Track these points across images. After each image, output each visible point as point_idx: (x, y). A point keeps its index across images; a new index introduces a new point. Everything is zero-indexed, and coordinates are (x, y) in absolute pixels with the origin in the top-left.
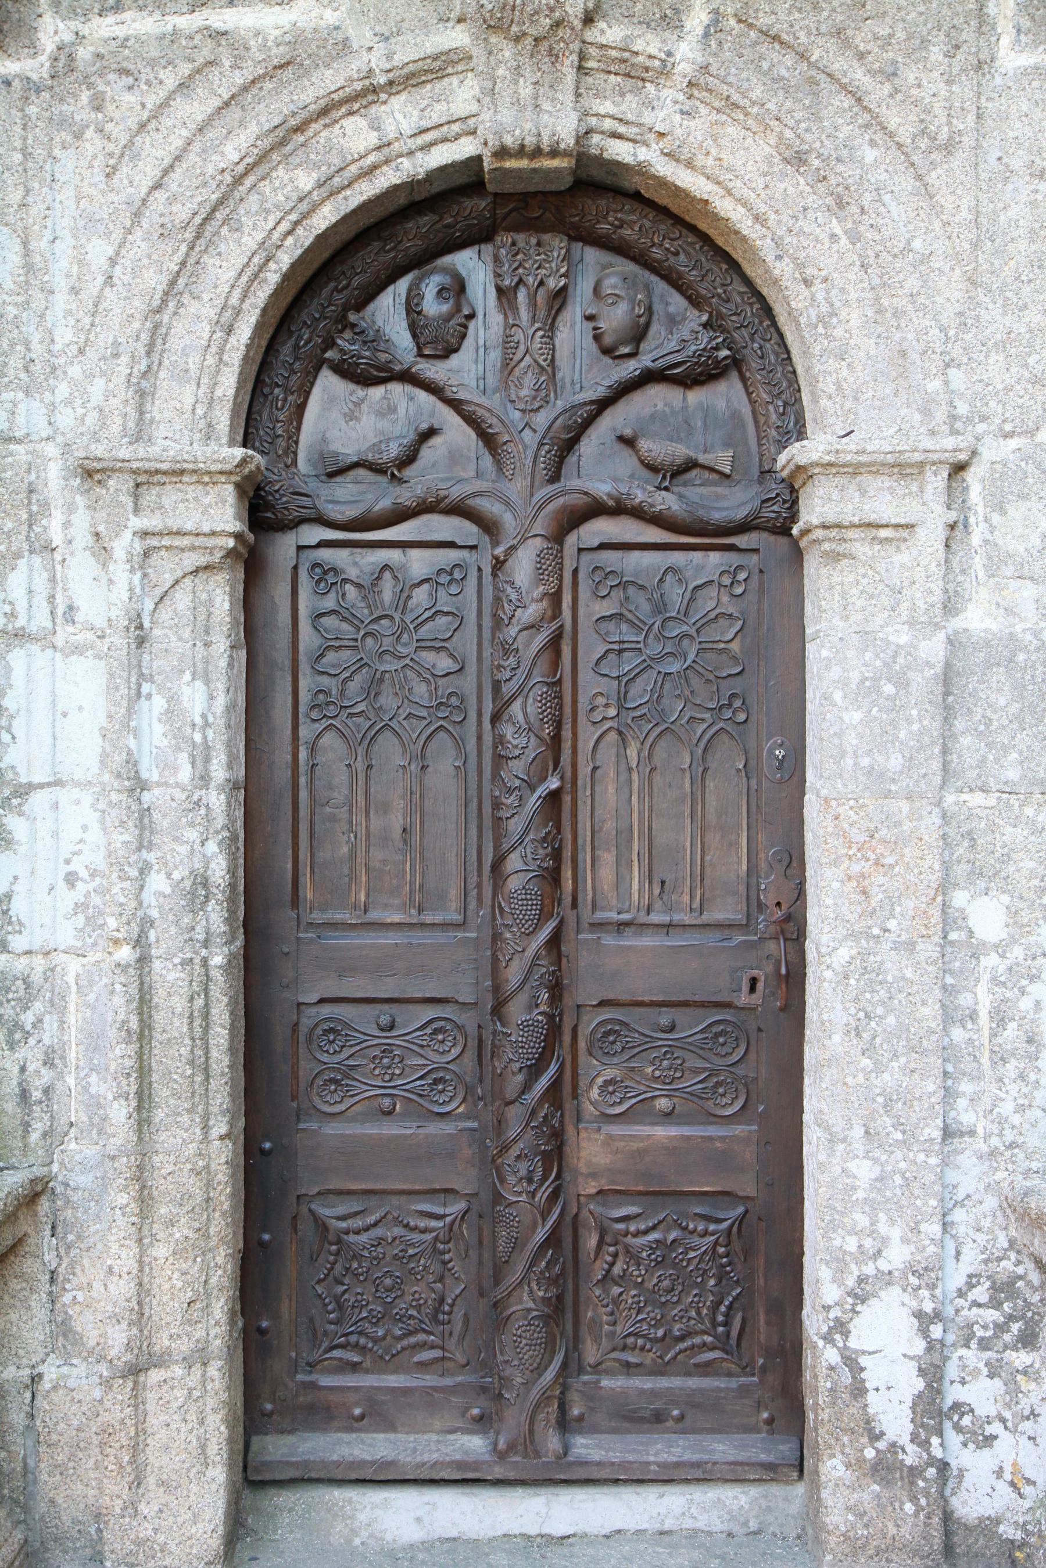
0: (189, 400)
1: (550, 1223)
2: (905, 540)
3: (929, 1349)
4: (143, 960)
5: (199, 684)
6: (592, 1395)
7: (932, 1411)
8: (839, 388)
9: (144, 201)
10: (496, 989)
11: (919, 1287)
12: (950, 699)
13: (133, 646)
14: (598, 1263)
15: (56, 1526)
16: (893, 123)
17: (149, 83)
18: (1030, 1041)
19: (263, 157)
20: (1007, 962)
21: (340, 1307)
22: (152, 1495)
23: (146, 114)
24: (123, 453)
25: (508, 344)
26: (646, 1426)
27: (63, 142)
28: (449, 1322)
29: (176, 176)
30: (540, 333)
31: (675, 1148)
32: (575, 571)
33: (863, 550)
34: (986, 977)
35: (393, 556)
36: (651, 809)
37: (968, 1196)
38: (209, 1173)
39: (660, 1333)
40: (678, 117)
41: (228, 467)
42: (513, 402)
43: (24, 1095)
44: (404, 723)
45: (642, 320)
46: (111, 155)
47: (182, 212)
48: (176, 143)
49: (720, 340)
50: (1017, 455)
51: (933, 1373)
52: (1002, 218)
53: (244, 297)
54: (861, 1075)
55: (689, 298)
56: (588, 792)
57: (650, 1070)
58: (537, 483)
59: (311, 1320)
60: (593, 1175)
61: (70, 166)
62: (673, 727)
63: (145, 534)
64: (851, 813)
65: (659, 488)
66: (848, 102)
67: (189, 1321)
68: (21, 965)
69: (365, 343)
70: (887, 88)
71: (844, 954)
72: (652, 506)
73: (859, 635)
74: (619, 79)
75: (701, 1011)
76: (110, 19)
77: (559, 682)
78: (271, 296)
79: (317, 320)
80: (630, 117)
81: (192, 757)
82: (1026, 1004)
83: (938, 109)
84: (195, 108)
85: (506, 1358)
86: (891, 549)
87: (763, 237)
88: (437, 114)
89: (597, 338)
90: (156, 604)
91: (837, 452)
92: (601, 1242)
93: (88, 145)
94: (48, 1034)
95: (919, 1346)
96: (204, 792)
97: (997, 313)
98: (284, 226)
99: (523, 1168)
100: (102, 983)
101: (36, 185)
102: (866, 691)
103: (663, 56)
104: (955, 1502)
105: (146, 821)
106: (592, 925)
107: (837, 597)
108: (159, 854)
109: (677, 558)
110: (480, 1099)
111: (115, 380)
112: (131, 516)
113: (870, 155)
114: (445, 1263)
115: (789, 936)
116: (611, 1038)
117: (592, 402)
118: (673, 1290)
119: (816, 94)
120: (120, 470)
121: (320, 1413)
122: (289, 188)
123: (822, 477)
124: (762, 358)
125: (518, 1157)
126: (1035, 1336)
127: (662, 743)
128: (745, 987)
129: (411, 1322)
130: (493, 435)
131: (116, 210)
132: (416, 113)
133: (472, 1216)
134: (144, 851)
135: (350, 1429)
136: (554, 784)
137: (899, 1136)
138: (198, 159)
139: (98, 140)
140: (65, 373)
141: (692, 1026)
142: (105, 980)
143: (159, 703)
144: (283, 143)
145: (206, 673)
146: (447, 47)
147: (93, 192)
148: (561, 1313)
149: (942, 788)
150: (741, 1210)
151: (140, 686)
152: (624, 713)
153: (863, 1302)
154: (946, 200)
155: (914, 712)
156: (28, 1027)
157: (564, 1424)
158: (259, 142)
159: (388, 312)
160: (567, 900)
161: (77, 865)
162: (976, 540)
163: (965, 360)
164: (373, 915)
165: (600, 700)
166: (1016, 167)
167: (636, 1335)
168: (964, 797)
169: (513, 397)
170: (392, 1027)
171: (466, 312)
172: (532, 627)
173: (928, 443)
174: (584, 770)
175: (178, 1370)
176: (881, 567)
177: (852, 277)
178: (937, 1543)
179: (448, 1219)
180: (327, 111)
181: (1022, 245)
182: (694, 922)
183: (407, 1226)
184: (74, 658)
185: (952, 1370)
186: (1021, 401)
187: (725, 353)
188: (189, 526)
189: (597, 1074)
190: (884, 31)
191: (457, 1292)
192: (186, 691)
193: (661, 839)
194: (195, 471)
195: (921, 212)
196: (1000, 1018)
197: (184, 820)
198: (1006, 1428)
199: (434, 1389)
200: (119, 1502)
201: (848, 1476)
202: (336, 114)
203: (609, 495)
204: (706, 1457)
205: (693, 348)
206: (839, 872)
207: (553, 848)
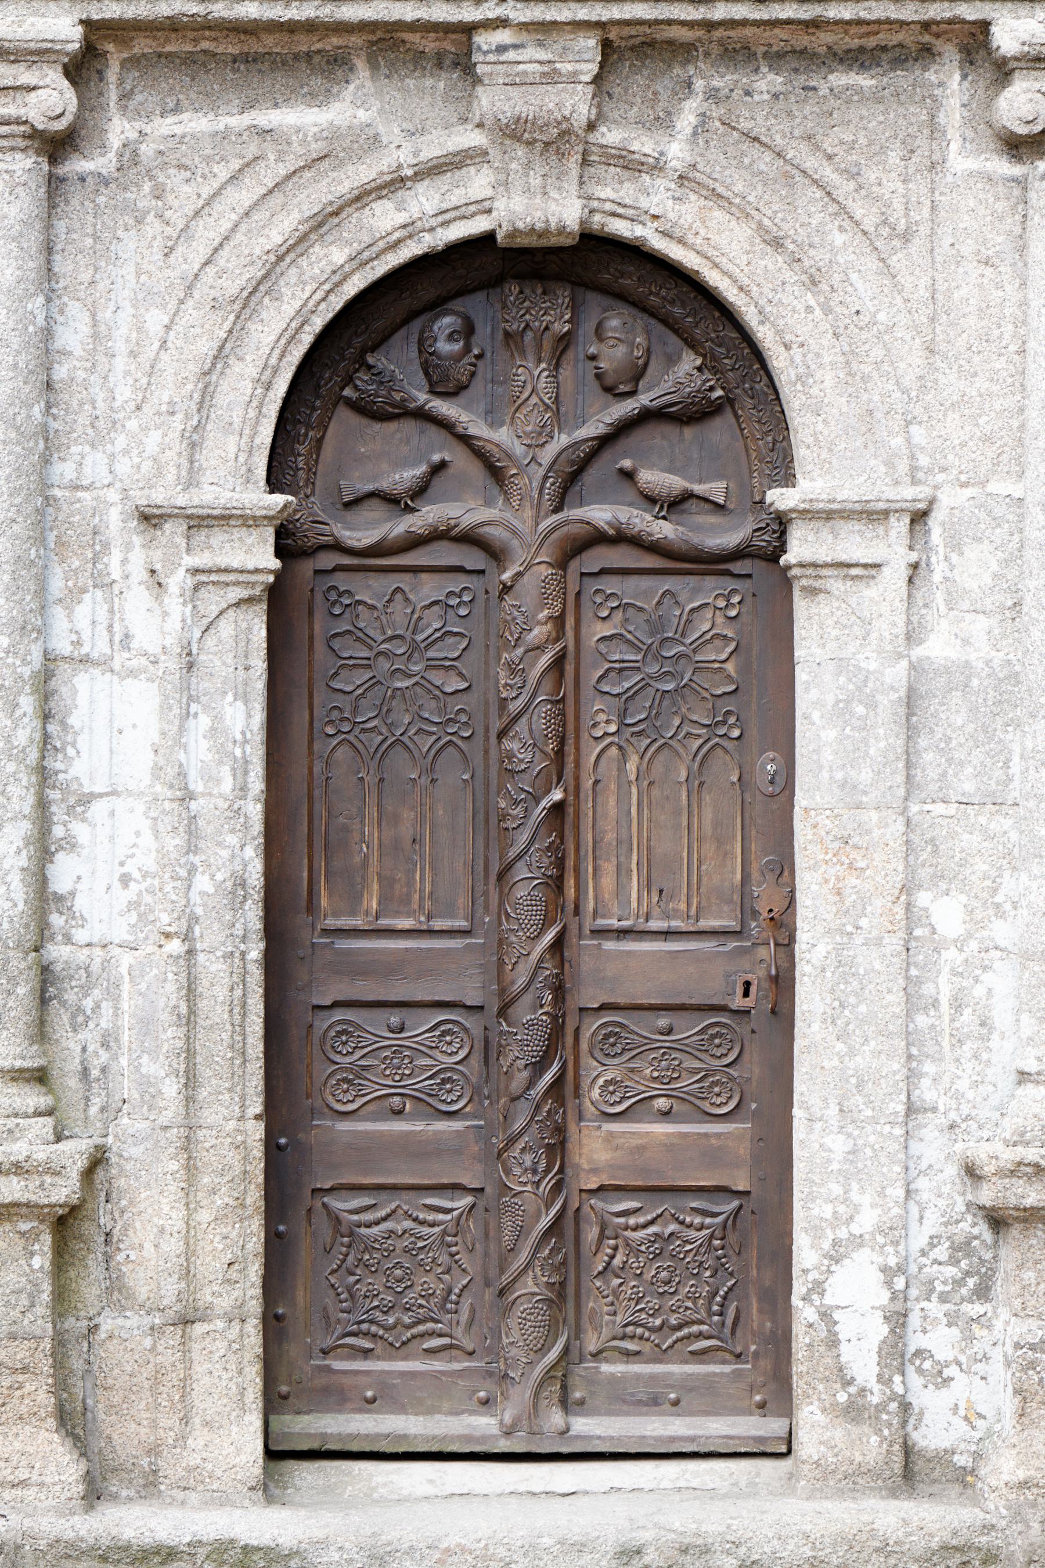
0: (232, 449)
1: (553, 1212)
2: (873, 577)
3: (894, 1298)
4: (191, 952)
5: (239, 704)
6: (591, 1381)
7: (896, 1354)
8: (816, 440)
10: (502, 991)
11: (884, 1246)
12: (914, 719)
13: (185, 671)
14: (599, 1255)
15: (113, 1459)
16: (858, 214)
17: (204, 177)
19: (303, 238)
20: (964, 955)
21: (352, 1296)
22: (197, 1433)
23: (201, 202)
24: (181, 501)
26: (645, 1409)
27: (126, 225)
29: (224, 253)
30: (546, 373)
31: (672, 1145)
32: (578, 594)
33: (836, 585)
35: (403, 581)
36: (650, 820)
37: (930, 1166)
38: (245, 1148)
39: (658, 1322)
40: (670, 202)
41: (272, 513)
42: (519, 437)
44: (415, 738)
45: (641, 362)
46: (169, 238)
48: (226, 225)
50: (971, 502)
51: (898, 1320)
52: (956, 295)
53: (282, 355)
54: (836, 1059)
55: (685, 340)
56: (590, 804)
57: (648, 1071)
58: (542, 514)
59: (325, 1309)
60: (594, 1171)
61: (132, 245)
63: (196, 571)
64: (827, 822)
66: (819, 194)
67: (228, 1280)
68: (82, 956)
70: (852, 185)
71: (822, 949)
72: (650, 535)
73: (839, 653)
74: (618, 169)
75: (697, 1014)
76: (170, 120)
80: (627, 201)
81: (234, 769)
82: (979, 991)
83: (897, 204)
84: (243, 196)
86: (861, 585)
87: (748, 305)
88: (456, 198)
89: (598, 376)
91: (811, 501)
92: (602, 1236)
93: (148, 228)
94: (104, 1019)
95: (885, 1297)
96: (242, 802)
97: (953, 377)
99: (528, 1159)
100: (152, 974)
101: (103, 264)
102: (842, 711)
104: (916, 1436)
105: (193, 827)
106: (592, 931)
107: (815, 627)
108: (204, 858)
110: (486, 1098)
112: (184, 555)
113: (839, 239)
114: (452, 1255)
115: (781, 941)
116: (612, 1040)
119: (792, 187)
120: (176, 516)
121: (335, 1395)
122: (324, 262)
125: (523, 1150)
126: (988, 1289)
127: (661, 757)
128: (740, 991)
129: (421, 1311)
130: (501, 468)
132: (437, 196)
133: (479, 1210)
135: (360, 1411)
136: (557, 795)
137: (869, 1113)
138: (244, 238)
139: (158, 225)
140: (123, 426)
141: (689, 1029)
142: (155, 971)
143: (204, 721)
144: (320, 225)
145: (245, 694)
146: (466, 146)
147: (152, 268)
148: (563, 1298)
149: (906, 799)
150: (735, 1204)
153: (837, 1262)
154: (906, 280)
156: (89, 1012)
157: (565, 1403)
160: (570, 907)
161: (130, 868)
162: (937, 577)
163: (926, 419)
164: (384, 922)
165: (602, 717)
166: (966, 254)
167: (635, 1324)
168: (927, 807)
170: (402, 1030)
171: (476, 352)
172: (538, 648)
175: (220, 1324)
176: (853, 601)
178: (898, 1468)
180: (361, 198)
181: (972, 320)
182: (692, 929)
183: (415, 1220)
184: (129, 680)
185: (914, 1320)
186: (974, 456)
187: (719, 393)
188: (236, 564)
189: (597, 1076)
190: (848, 138)
191: (465, 1282)
192: (229, 711)
193: (661, 848)
195: (885, 289)
196: (958, 1006)
197: (226, 827)
198: (961, 1370)
199: (443, 1373)
200: (172, 1434)
201: (820, 1418)
204: (700, 1433)
205: (688, 390)
206: (817, 876)
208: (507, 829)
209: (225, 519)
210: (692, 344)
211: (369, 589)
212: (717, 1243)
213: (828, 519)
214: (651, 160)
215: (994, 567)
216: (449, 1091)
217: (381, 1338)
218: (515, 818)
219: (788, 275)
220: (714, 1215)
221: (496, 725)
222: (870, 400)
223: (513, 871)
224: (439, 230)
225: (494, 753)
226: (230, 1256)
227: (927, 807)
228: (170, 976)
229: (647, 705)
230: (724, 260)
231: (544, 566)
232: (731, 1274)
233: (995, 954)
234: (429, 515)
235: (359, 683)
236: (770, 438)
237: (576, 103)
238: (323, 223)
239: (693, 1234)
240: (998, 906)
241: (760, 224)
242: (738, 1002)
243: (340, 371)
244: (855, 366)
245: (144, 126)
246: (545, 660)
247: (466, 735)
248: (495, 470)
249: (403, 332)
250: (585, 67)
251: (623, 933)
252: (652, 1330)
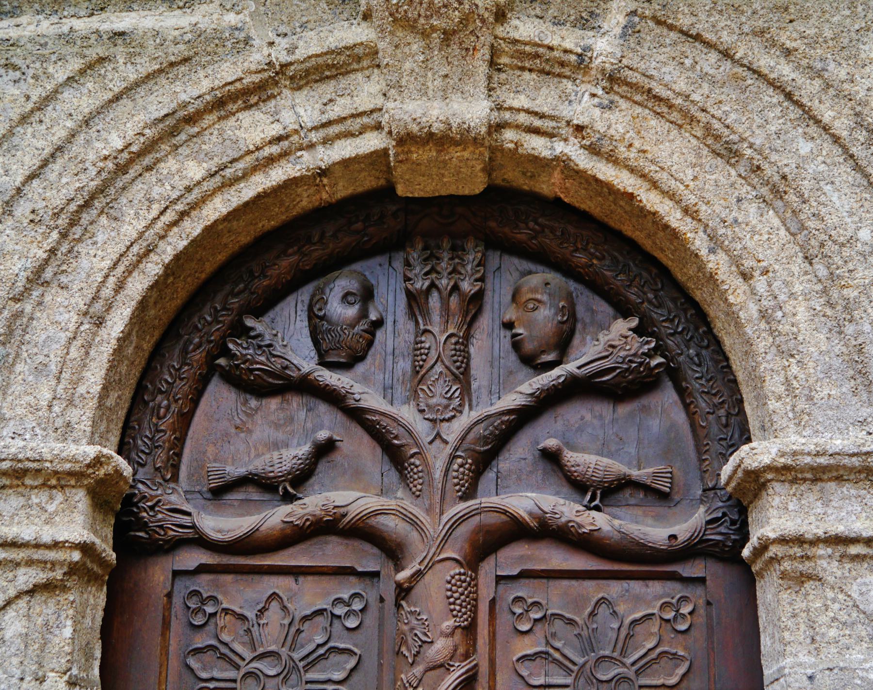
9: (19, 190)
16: (827, 116)
17: (35, 77)
19: (150, 147)
23: (30, 106)
25: (417, 352)
30: (453, 340)
32: (493, 602)
41: (77, 467)
47: (57, 199)
48: (60, 134)
49: (653, 345)
65: (589, 508)
66: (778, 98)
69: (260, 347)
72: (580, 526)
84: (82, 100)
89: (517, 345)
91: (795, 453)
103: (579, 51)
107: (803, 627)
109: (614, 589)
113: (805, 148)
117: (510, 412)
123: (777, 486)
130: (402, 446)
144: (173, 132)
146: (351, 42)
158: (147, 131)
169: (423, 406)
171: (373, 316)
172: (441, 666)
177: (795, 269)
194: (38, 471)
195: (866, 204)
203: (530, 514)
205: (623, 353)
210: (623, 310)
211: (241, 595)
213: (815, 480)
214: (573, 58)
224: (320, 149)
230: (665, 175)
231: (449, 564)
234: (314, 502)
236: (722, 412)
238: (179, 126)
241: (708, 128)
244: (835, 294)
248: (396, 454)
249: (291, 300)
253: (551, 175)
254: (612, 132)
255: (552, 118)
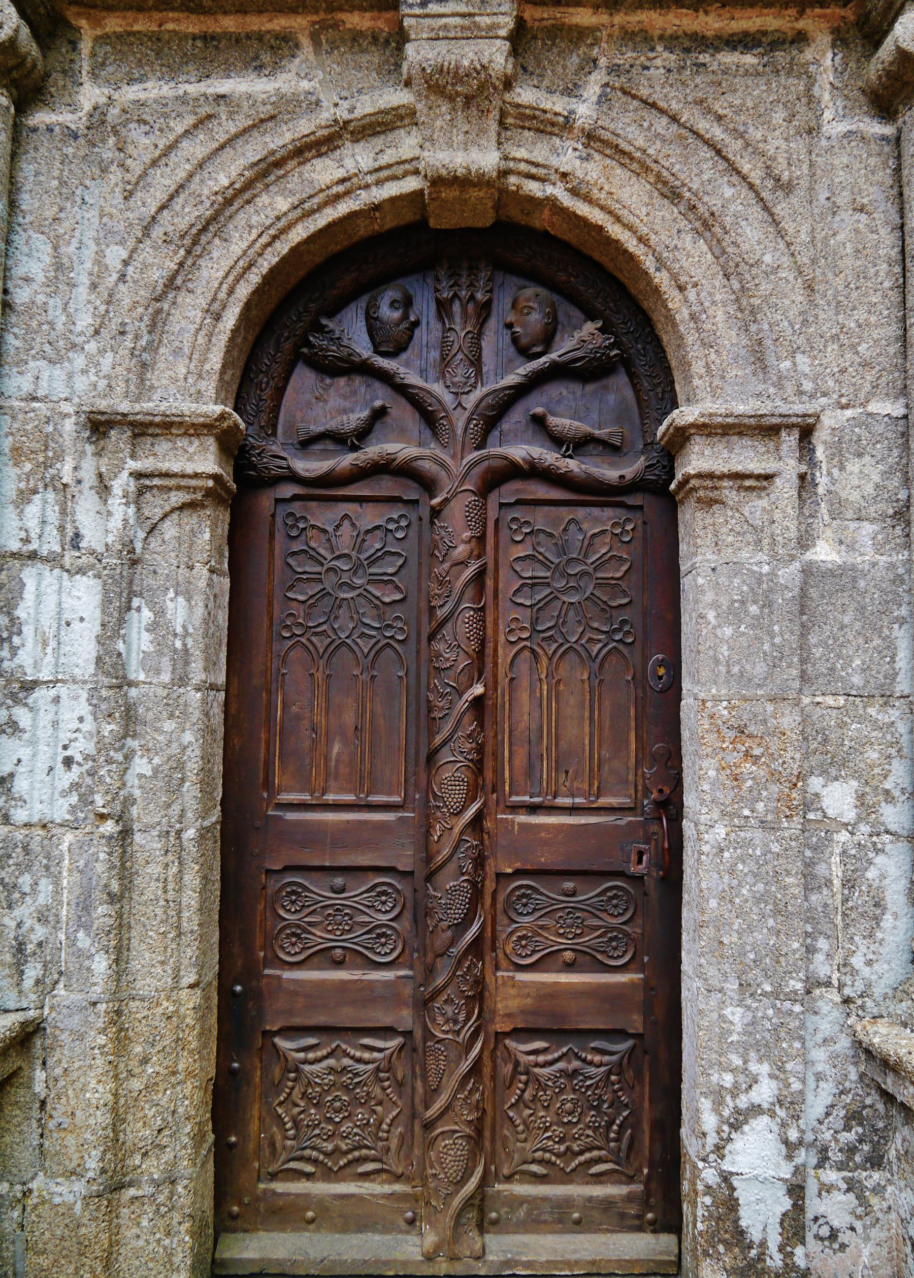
2: (765, 488)
4: (126, 833)
5: (180, 599)
9: (154, 218)
16: (746, 168)
17: (161, 130)
18: (877, 905)
19: (249, 185)
23: (158, 153)
24: (124, 407)
25: (444, 344)
28: (387, 1139)
29: (180, 200)
32: (497, 521)
34: (838, 850)
39: (562, 1148)
40: (578, 162)
43: (20, 948)
48: (181, 174)
53: (231, 292)
62: (575, 646)
63: (138, 475)
64: (725, 712)
65: (564, 456)
66: (710, 154)
69: (332, 339)
72: (558, 468)
76: (136, 87)
77: (482, 609)
78: (254, 293)
79: (295, 322)
82: (871, 874)
84: (196, 148)
85: (434, 1172)
90: (148, 533)
91: (711, 415)
93: (111, 176)
98: (265, 239)
107: (710, 536)
108: (143, 742)
111: (121, 352)
113: (728, 192)
117: (510, 388)
118: (573, 1112)
120: (120, 423)
124: (644, 356)
125: (446, 1001)
128: (634, 858)
131: (131, 224)
134: (129, 739)
136: (478, 689)
140: (83, 348)
144: (265, 174)
146: (396, 104)
151: (130, 601)
152: (535, 635)
154: (789, 226)
155: (776, 628)
158: (246, 173)
159: (354, 334)
162: (821, 490)
169: (448, 383)
170: (343, 891)
171: (412, 319)
172: (462, 563)
173: (784, 409)
174: (503, 682)
177: (717, 283)
179: (388, 1052)
181: (848, 262)
183: (352, 1058)
184: (78, 577)
185: (812, 1187)
191: (394, 1113)
194: (181, 423)
196: (849, 883)
202: (308, 155)
203: (524, 459)
205: (590, 346)
207: (478, 744)
208: (434, 719)
209: (168, 427)
211: (324, 516)
212: (613, 1078)
214: (561, 119)
215: (876, 478)
216: (383, 945)
217: (322, 1162)
218: (442, 708)
219: (683, 224)
220: (611, 1053)
221: (426, 631)
222: (760, 331)
223: (439, 755)
224: (374, 188)
225: (424, 656)
226: (159, 1122)
227: (818, 699)
228: (102, 856)
229: (555, 614)
232: (626, 1106)
233: (887, 838)
234: (373, 451)
235: (311, 593)
236: (659, 390)
237: (496, 55)
238: (269, 169)
239: (593, 1070)
240: (887, 792)
241: (659, 176)
242: (633, 869)
243: (292, 319)
245: (112, 92)
246: (469, 572)
247: (401, 638)
248: (430, 418)
250: (502, 20)
251: (533, 809)
252: (558, 1155)
253: (542, 212)
254: (588, 178)
255: (544, 166)
